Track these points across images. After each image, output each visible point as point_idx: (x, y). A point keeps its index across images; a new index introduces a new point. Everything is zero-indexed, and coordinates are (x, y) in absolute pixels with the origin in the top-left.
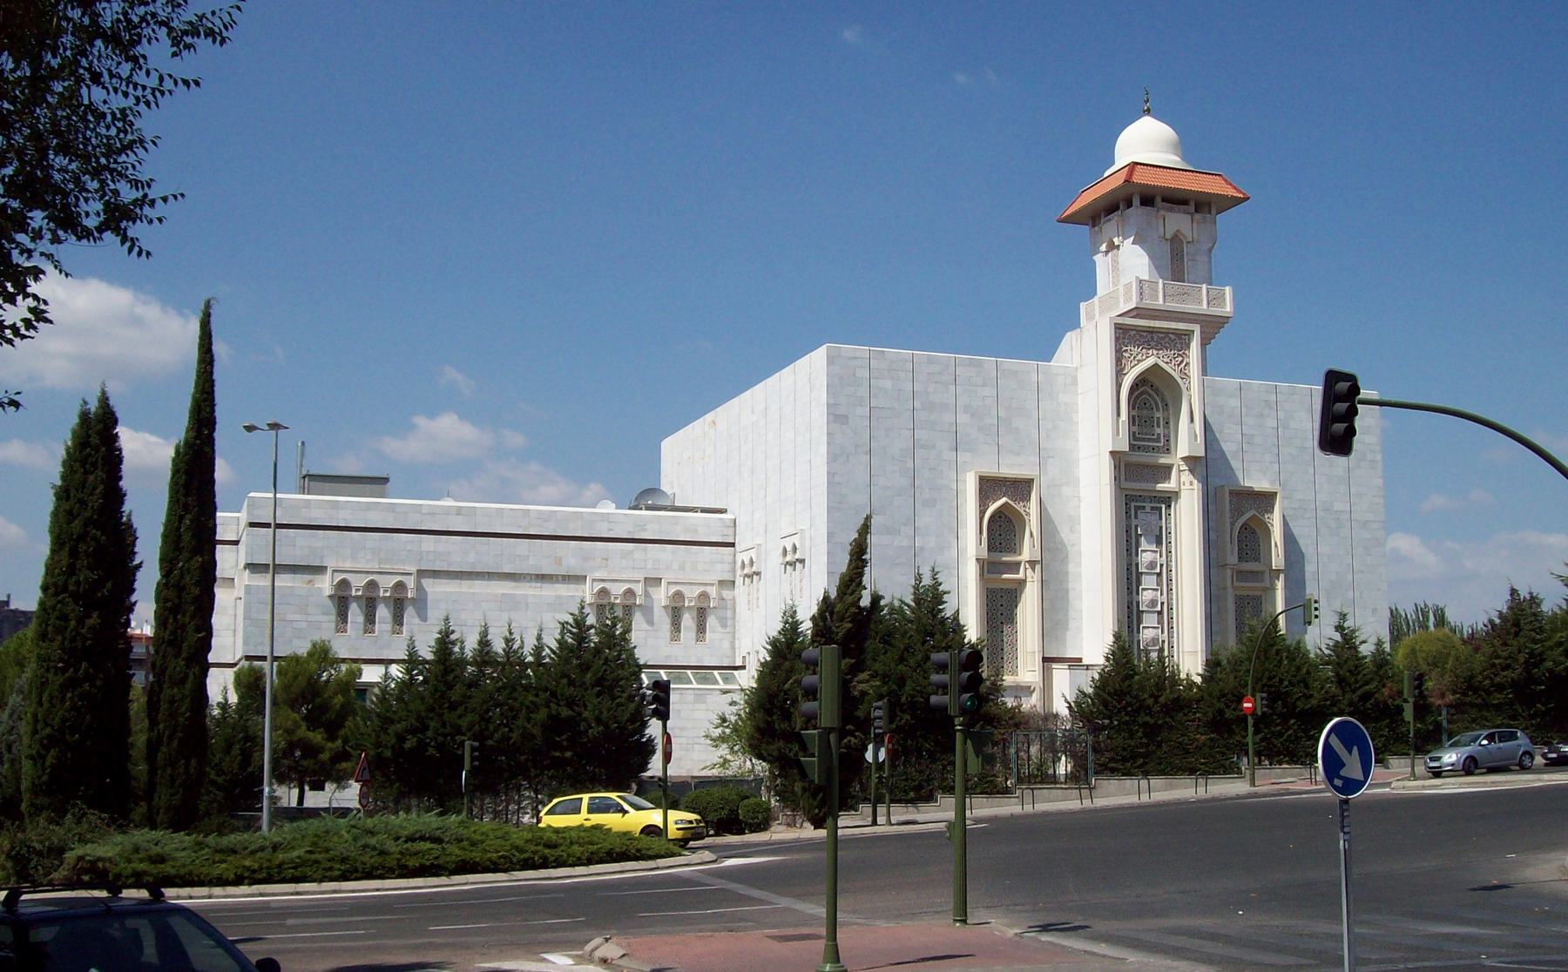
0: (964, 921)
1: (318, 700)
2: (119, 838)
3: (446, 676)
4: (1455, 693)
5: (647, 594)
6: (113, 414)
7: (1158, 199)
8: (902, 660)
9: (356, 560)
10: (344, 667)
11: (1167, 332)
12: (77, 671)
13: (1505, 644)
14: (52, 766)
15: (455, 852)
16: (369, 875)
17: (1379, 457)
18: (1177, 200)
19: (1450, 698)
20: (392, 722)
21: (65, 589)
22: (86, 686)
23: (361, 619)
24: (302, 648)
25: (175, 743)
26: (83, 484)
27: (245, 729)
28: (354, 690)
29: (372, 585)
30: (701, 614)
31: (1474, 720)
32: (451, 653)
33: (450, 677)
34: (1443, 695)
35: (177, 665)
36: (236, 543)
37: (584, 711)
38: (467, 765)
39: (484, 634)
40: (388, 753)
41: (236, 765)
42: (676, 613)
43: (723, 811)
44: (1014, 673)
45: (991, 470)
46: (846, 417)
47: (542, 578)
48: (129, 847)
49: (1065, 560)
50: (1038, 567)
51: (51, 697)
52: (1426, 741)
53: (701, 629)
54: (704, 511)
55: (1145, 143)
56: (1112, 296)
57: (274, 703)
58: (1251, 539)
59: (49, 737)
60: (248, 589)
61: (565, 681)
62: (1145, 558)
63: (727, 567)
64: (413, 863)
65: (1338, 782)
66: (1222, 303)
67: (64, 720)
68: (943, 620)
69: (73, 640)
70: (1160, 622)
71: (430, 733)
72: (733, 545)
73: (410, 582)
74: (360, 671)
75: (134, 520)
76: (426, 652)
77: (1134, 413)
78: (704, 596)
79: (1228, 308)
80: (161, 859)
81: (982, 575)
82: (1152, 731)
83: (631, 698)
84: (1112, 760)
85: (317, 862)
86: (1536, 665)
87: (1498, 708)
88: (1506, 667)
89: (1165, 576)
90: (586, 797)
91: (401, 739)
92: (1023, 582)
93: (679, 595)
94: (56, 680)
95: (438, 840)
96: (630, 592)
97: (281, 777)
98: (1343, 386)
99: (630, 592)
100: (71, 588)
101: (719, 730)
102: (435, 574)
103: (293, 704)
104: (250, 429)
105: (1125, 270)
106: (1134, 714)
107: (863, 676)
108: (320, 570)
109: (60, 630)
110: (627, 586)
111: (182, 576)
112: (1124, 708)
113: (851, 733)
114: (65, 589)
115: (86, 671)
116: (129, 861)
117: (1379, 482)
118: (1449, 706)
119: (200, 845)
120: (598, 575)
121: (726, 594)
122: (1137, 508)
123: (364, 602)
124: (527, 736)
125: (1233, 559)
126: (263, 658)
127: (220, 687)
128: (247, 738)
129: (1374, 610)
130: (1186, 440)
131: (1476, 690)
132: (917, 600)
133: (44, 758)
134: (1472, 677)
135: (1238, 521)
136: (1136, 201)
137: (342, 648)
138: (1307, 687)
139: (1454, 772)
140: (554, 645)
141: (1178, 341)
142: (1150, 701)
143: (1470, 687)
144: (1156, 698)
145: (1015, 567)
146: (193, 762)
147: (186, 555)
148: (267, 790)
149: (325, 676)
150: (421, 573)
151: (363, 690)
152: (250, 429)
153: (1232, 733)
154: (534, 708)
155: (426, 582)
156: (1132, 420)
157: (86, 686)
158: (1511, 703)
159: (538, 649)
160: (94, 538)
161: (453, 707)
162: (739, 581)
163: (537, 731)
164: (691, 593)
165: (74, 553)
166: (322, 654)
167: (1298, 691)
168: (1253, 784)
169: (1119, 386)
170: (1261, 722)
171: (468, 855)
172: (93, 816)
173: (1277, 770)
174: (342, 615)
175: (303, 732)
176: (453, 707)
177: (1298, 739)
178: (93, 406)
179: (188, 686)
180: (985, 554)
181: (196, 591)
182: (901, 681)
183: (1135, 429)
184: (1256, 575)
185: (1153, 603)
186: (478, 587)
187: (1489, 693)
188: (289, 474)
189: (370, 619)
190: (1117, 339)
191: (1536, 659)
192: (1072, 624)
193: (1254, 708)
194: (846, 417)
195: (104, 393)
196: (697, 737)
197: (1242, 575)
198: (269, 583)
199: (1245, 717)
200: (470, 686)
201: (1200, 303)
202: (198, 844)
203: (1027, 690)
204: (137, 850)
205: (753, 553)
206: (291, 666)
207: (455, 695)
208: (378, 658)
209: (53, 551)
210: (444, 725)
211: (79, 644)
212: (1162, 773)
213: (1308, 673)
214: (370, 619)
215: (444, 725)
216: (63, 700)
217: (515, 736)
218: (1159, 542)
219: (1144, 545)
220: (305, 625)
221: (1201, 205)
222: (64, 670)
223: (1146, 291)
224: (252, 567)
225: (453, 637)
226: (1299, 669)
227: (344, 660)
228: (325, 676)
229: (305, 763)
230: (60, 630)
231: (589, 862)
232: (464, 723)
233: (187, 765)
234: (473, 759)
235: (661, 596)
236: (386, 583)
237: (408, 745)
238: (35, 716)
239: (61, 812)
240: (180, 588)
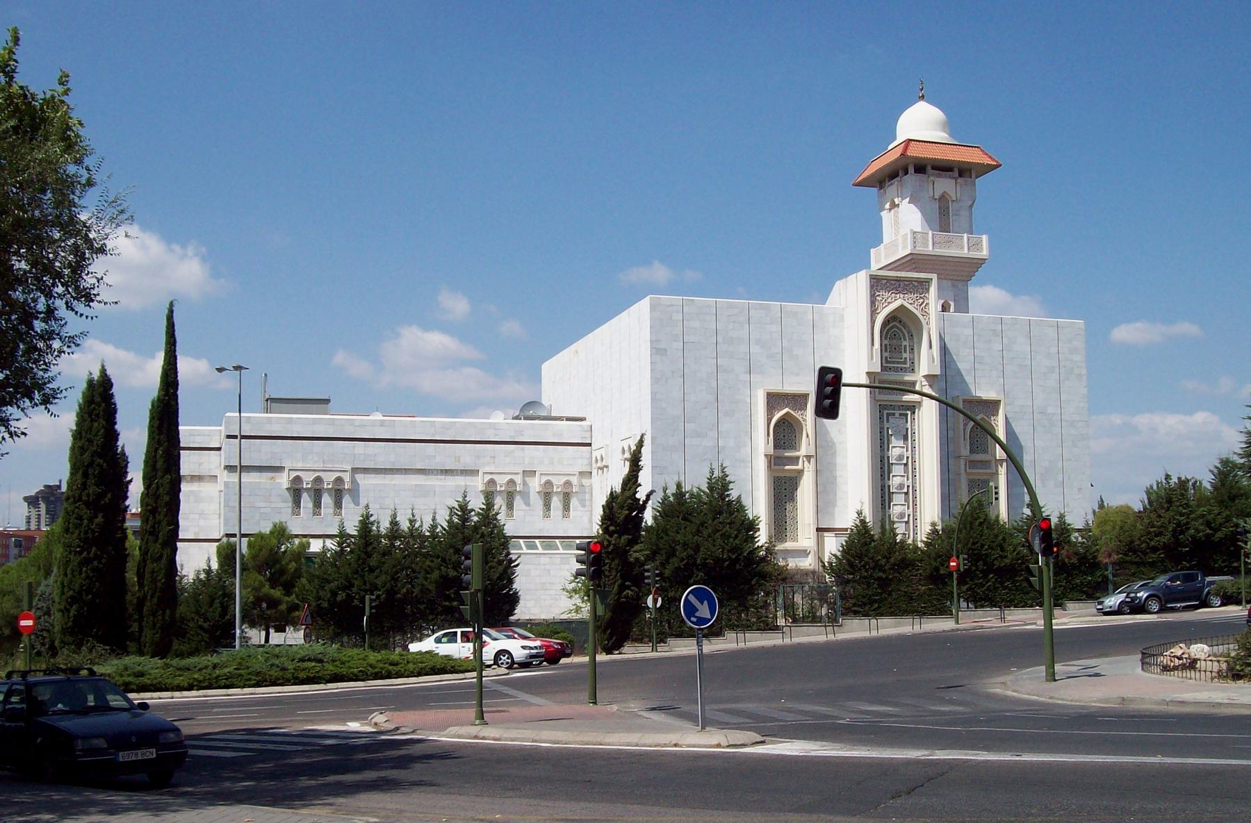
0: (595, 703)
1: (278, 566)
2: (115, 662)
3: (366, 545)
4: (1118, 553)
5: (525, 483)
6: (109, 380)
7: (929, 168)
8: (698, 532)
9: (306, 461)
10: (297, 541)
11: (910, 280)
12: (89, 553)
13: (1160, 516)
14: (75, 616)
15: (330, 668)
16: (274, 684)
17: (1084, 372)
18: (943, 168)
19: (1115, 557)
20: (329, 582)
21: (80, 499)
22: (95, 563)
23: (311, 505)
24: (266, 528)
25: (155, 600)
26: (90, 429)
27: (224, 587)
28: (301, 555)
29: (318, 480)
30: (567, 498)
31: (1133, 574)
32: (371, 531)
33: (370, 548)
34: (1110, 555)
35: (156, 548)
36: (219, 449)
37: (457, 574)
38: (367, 612)
39: (394, 516)
40: (325, 605)
41: (217, 614)
42: (547, 496)
43: (558, 641)
44: (795, 539)
45: (777, 388)
46: (666, 350)
47: (446, 472)
48: (121, 667)
49: (834, 454)
50: (813, 460)
51: (73, 571)
52: (1094, 591)
53: (566, 508)
54: (568, 419)
55: (920, 124)
56: (894, 244)
57: (243, 569)
58: (982, 434)
59: (72, 597)
60: (226, 484)
61: (451, 551)
62: (894, 453)
63: (586, 462)
64: (303, 675)
65: (693, 619)
66: (980, 249)
67: (82, 586)
68: (730, 502)
69: (86, 533)
70: (907, 500)
71: (355, 590)
72: (590, 445)
73: (347, 477)
74: (309, 544)
75: (126, 450)
76: (352, 529)
77: (886, 342)
78: (568, 484)
79: (984, 253)
80: (142, 674)
81: (769, 466)
82: (884, 583)
83: (500, 563)
84: (854, 605)
85: (240, 675)
86: (1182, 532)
87: (1152, 564)
88: (1160, 534)
89: (910, 466)
90: (459, 631)
91: (334, 594)
92: (801, 472)
93: (549, 483)
94: (75, 559)
95: (320, 661)
96: (512, 482)
97: (251, 620)
98: (830, 376)
99: (512, 482)
100: (84, 498)
101: (573, 585)
102: (366, 471)
103: (259, 569)
104: (220, 370)
105: (903, 225)
106: (876, 571)
107: (637, 547)
108: (279, 469)
109: (77, 526)
110: (510, 477)
111: (158, 488)
112: (864, 566)
113: (628, 587)
114: (80, 499)
115: (95, 554)
116: (122, 676)
117: (1085, 391)
118: (1114, 564)
119: (167, 666)
120: (487, 469)
121: (585, 482)
122: (888, 415)
123: (312, 493)
124: (425, 591)
125: (965, 451)
126: (234, 536)
127: (194, 561)
128: (224, 595)
129: (1080, 489)
130: (927, 362)
131: (1135, 552)
132: (711, 488)
133: (68, 611)
134: (1132, 542)
135: (970, 423)
136: (911, 170)
137: (295, 527)
138: (1003, 550)
139: (1118, 612)
140: (445, 525)
141: (921, 287)
142: (883, 562)
143: (1129, 550)
144: (888, 559)
145: (795, 460)
146: (168, 612)
147: (159, 474)
148: (238, 632)
149: (283, 548)
150: (355, 470)
151: (310, 558)
152: (220, 370)
153: (945, 584)
154: (429, 571)
155: (359, 477)
156: (884, 348)
157: (95, 563)
158: (1163, 561)
159: (434, 527)
160: (99, 465)
161: (372, 570)
162: (594, 472)
163: (432, 587)
164: (558, 482)
165: (85, 475)
166: (280, 533)
167: (996, 553)
168: (957, 622)
169: (873, 322)
170: (963, 577)
171: (338, 671)
172: (100, 648)
173: (980, 612)
174: (297, 503)
175: (267, 589)
176: (372, 570)
177: (996, 588)
178: (96, 375)
179: (164, 560)
180: (771, 451)
181: (167, 498)
182: (697, 549)
183: (886, 354)
184: (985, 464)
185: (901, 486)
186: (398, 480)
187: (1145, 554)
188: (254, 395)
189: (317, 504)
190: (872, 287)
191: (1181, 529)
192: (839, 503)
193: (958, 565)
194: (666, 350)
195: (103, 366)
196: (549, 587)
197: (973, 464)
198: (237, 480)
199: (951, 574)
200: (384, 555)
201: (962, 248)
202: (166, 664)
203: (804, 553)
204: (126, 669)
205: (602, 452)
206: (257, 540)
207: (373, 561)
208: (320, 531)
209: (72, 474)
210: (365, 584)
211: (90, 536)
212: (892, 614)
213: (1004, 539)
214: (317, 504)
215: (365, 584)
216: (80, 573)
217: (416, 591)
218: (905, 438)
219: (895, 442)
220: (268, 509)
221: (963, 171)
222: (80, 553)
223: (919, 240)
224: (230, 468)
225: (372, 519)
226: (996, 536)
227: (297, 536)
228: (283, 548)
229: (269, 612)
230: (77, 526)
231: (419, 675)
232: (379, 582)
233: (164, 614)
234: (371, 608)
235: (535, 484)
236: (329, 478)
237: (339, 598)
238: (62, 584)
239: (79, 645)
240: (156, 497)
